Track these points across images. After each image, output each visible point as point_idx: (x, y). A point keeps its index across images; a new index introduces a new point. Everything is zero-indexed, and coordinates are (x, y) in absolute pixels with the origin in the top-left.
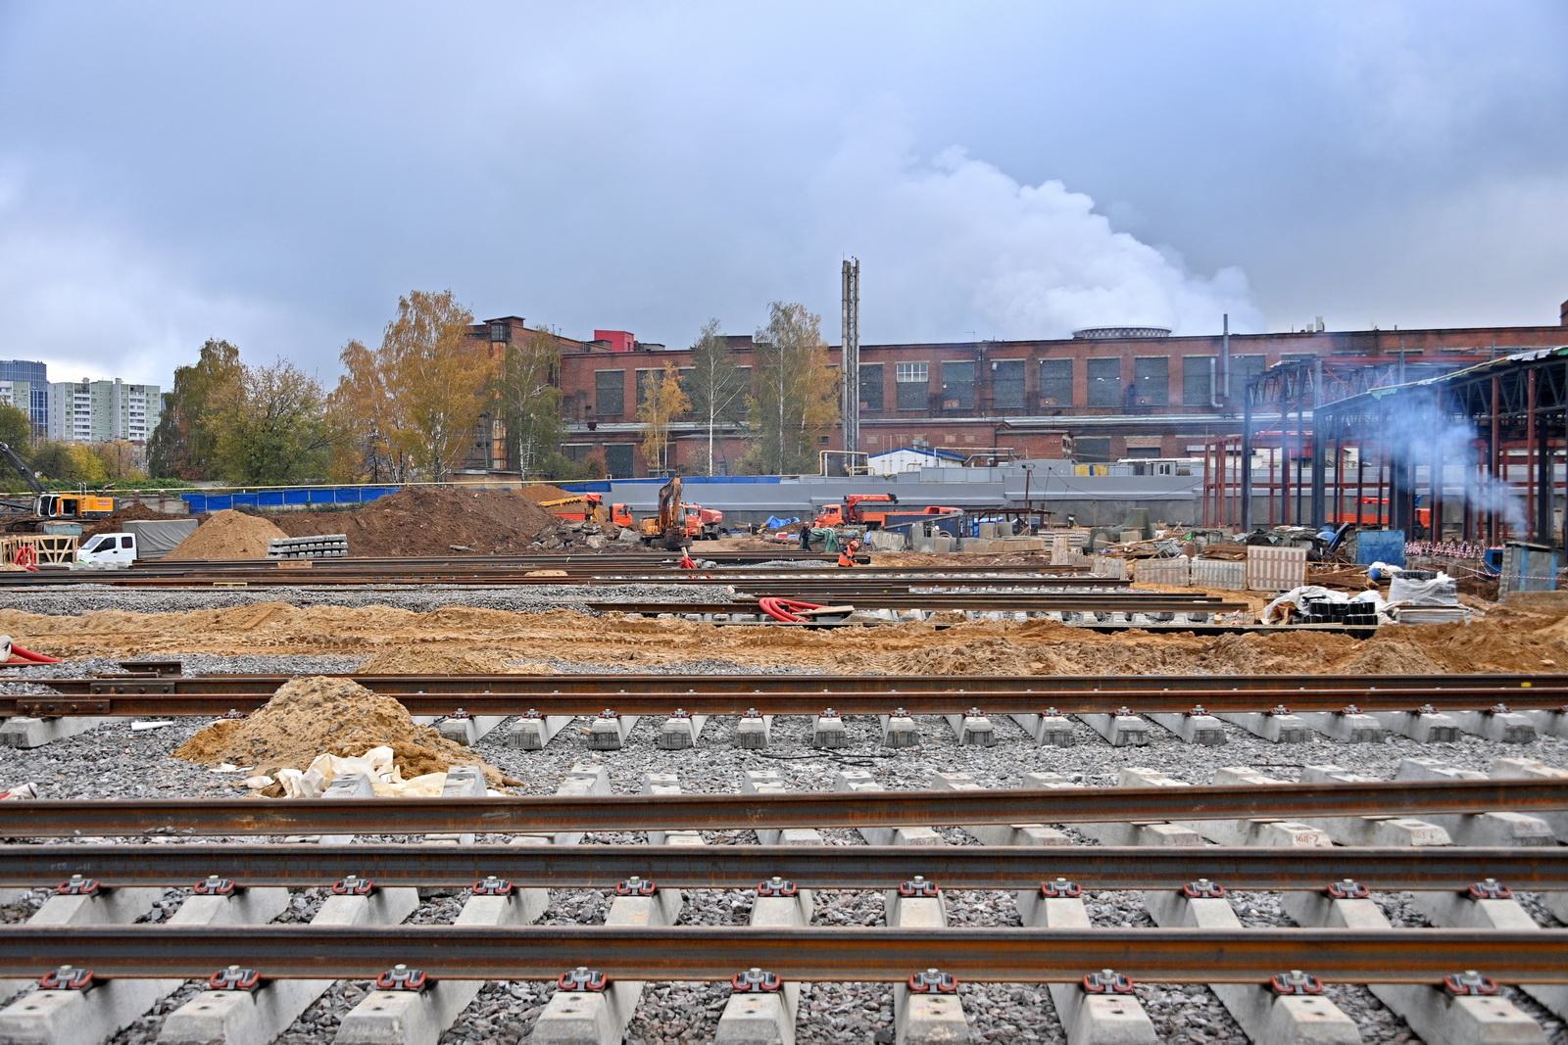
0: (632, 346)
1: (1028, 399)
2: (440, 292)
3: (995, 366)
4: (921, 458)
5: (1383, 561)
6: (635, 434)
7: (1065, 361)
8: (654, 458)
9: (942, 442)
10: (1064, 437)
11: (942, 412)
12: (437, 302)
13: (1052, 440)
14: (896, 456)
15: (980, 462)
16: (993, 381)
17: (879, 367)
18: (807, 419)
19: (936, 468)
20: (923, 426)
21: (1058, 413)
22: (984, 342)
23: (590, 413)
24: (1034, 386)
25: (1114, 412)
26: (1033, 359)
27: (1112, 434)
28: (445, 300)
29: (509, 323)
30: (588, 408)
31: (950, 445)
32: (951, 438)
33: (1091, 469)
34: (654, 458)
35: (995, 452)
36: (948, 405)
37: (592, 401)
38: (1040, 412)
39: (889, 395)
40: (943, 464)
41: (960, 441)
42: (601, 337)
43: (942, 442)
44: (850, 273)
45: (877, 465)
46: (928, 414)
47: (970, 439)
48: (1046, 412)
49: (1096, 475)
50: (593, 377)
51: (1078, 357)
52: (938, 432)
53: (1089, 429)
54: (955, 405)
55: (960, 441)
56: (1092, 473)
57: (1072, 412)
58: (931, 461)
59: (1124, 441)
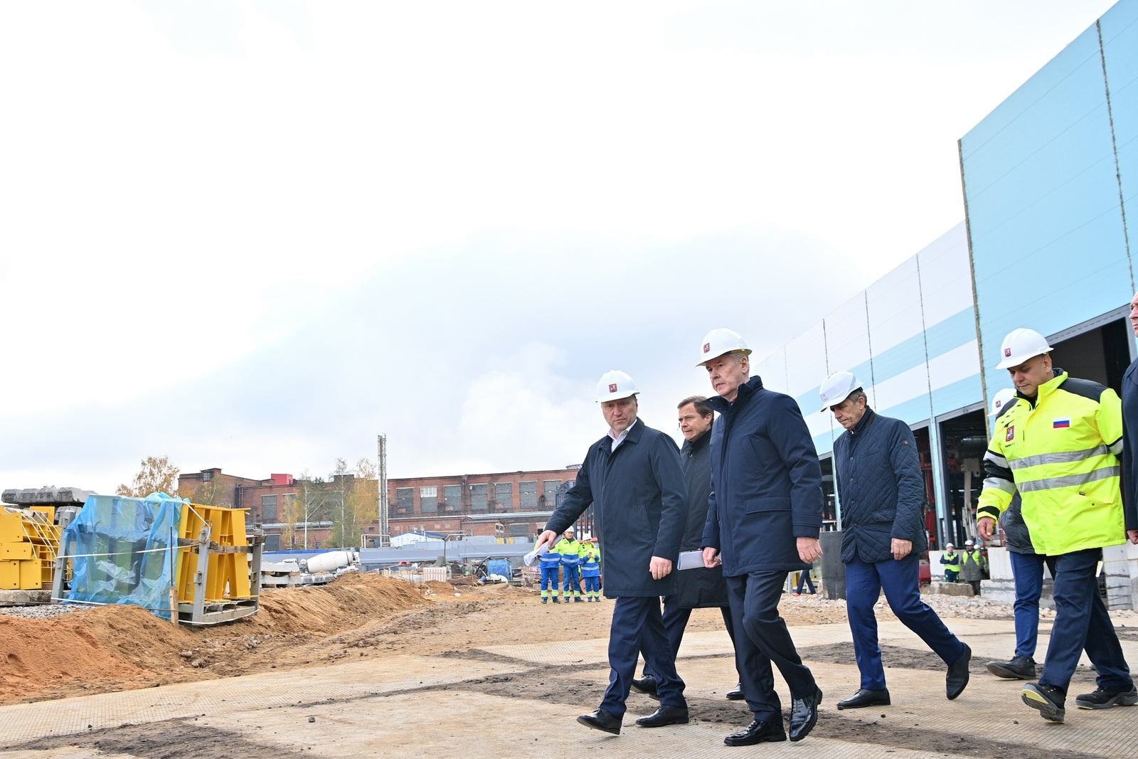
0: (292, 482)
1: (489, 505)
2: (162, 457)
3: (471, 488)
4: (418, 537)
5: (1059, 623)
6: (279, 529)
7: (508, 484)
8: (288, 541)
9: (433, 529)
10: (497, 524)
11: (445, 513)
12: (161, 462)
13: (490, 525)
14: (405, 536)
15: (452, 539)
16: (471, 495)
17: (411, 490)
18: (356, 518)
19: (426, 542)
20: (424, 520)
21: (505, 512)
22: (466, 475)
23: (259, 518)
24: (492, 498)
25: (483, 511)
26: (491, 483)
27: (530, 522)
28: (164, 462)
29: (212, 472)
30: (258, 516)
31: (437, 530)
32: (437, 526)
33: (505, 540)
34: (288, 541)
35: (461, 533)
36: (448, 509)
37: (260, 513)
38: (496, 511)
39: (416, 505)
40: (429, 540)
41: (443, 527)
42: (275, 477)
43: (433, 529)
44: (382, 441)
45: (395, 541)
46: (437, 514)
47: (448, 526)
48: (498, 511)
49: (508, 543)
50: (261, 499)
51: (514, 481)
52: (431, 523)
53: (517, 519)
54: (452, 509)
55: (443, 527)
56: (505, 542)
57: (512, 510)
58: (423, 538)
59: (535, 526)
